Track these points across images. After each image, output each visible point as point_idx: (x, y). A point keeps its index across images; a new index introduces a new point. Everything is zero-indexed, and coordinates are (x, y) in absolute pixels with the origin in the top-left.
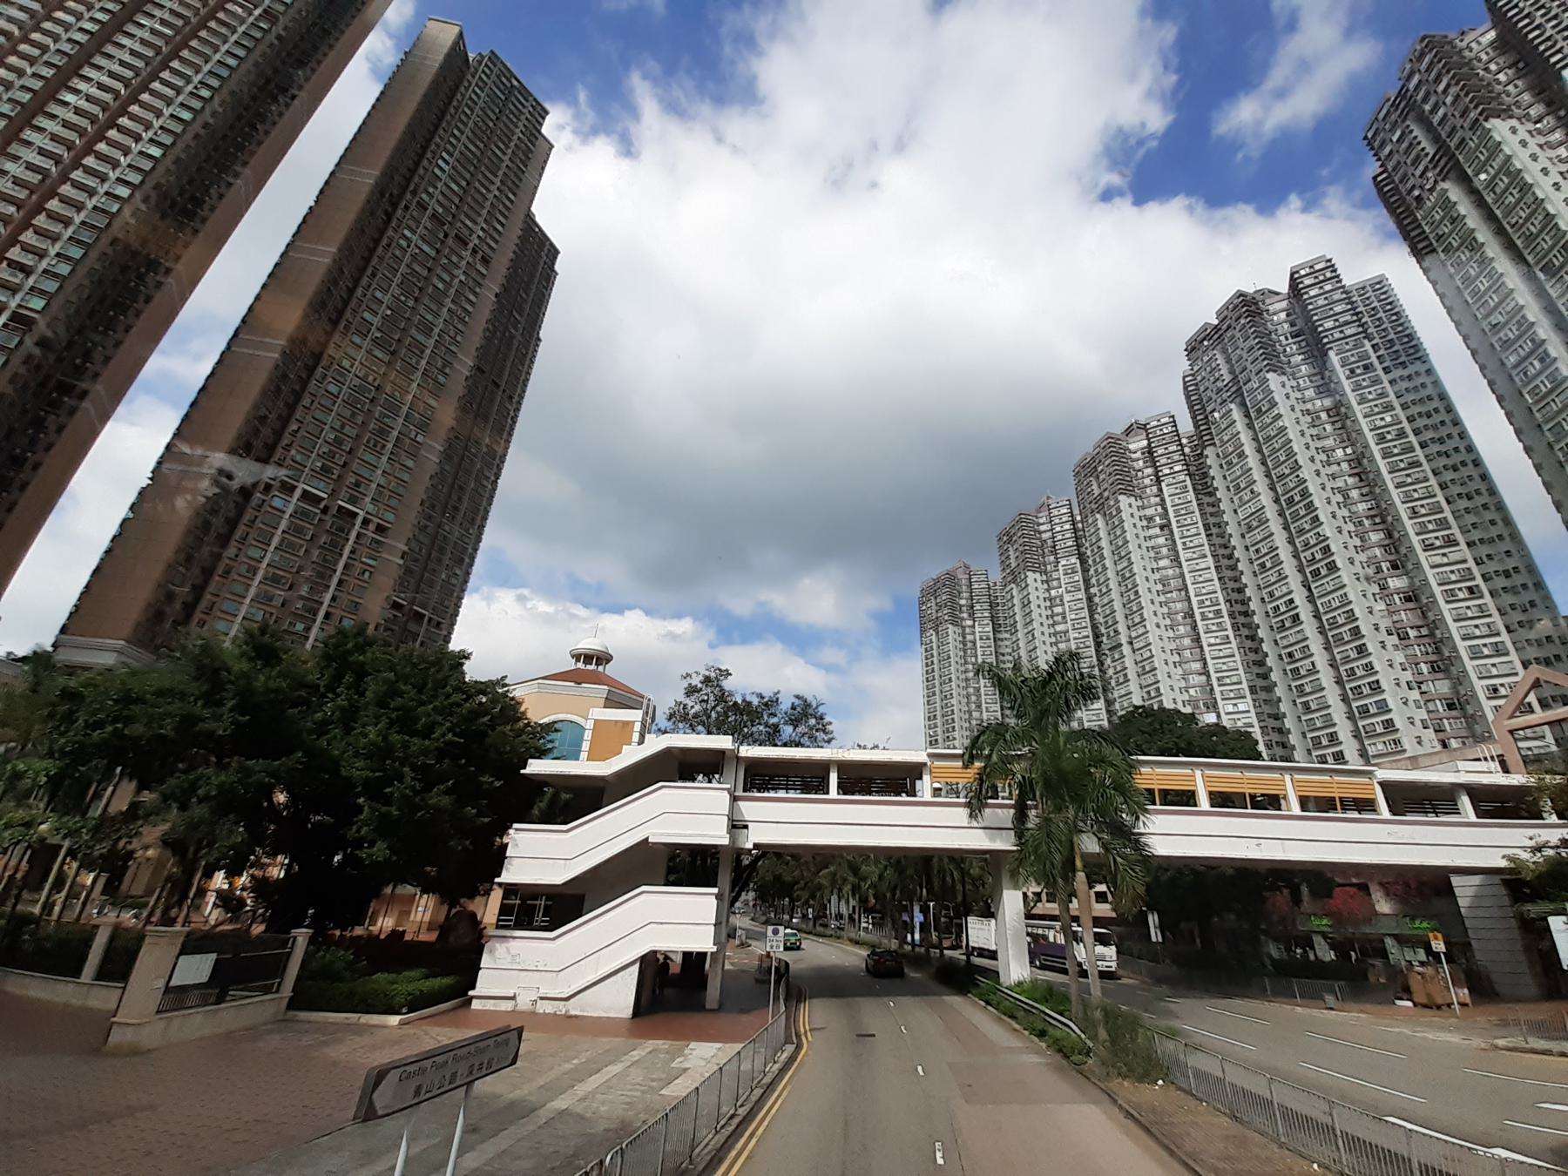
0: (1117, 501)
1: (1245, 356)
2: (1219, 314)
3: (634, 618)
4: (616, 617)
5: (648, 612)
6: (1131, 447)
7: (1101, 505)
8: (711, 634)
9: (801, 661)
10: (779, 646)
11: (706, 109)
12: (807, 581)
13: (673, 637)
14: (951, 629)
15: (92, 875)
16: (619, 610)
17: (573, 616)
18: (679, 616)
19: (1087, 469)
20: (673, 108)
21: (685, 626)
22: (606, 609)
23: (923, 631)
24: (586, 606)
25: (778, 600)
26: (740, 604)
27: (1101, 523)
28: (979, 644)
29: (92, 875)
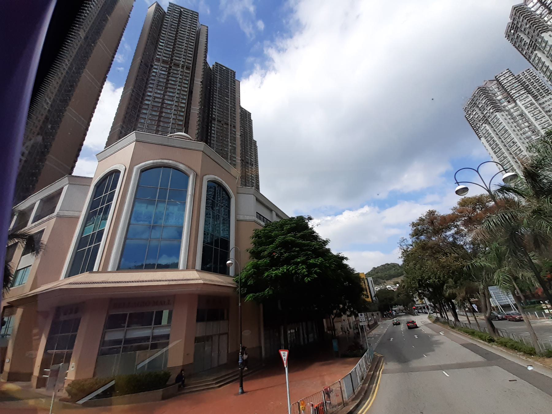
0: (542, 38)
1: (527, 51)
2: (511, 17)
3: (346, 214)
4: (340, 216)
5: (350, 209)
6: (529, 6)
7: (534, 46)
8: (377, 208)
9: (419, 205)
10: (406, 202)
11: (289, 42)
12: (406, 176)
13: (363, 214)
14: (498, 115)
15: (311, 340)
16: (341, 213)
17: (327, 221)
18: (362, 206)
19: (513, 31)
20: (280, 50)
21: (366, 209)
22: (336, 215)
23: (476, 130)
24: (330, 216)
25: (396, 186)
26: (383, 195)
27: (539, 54)
28: (526, 111)
29: (311, 340)
